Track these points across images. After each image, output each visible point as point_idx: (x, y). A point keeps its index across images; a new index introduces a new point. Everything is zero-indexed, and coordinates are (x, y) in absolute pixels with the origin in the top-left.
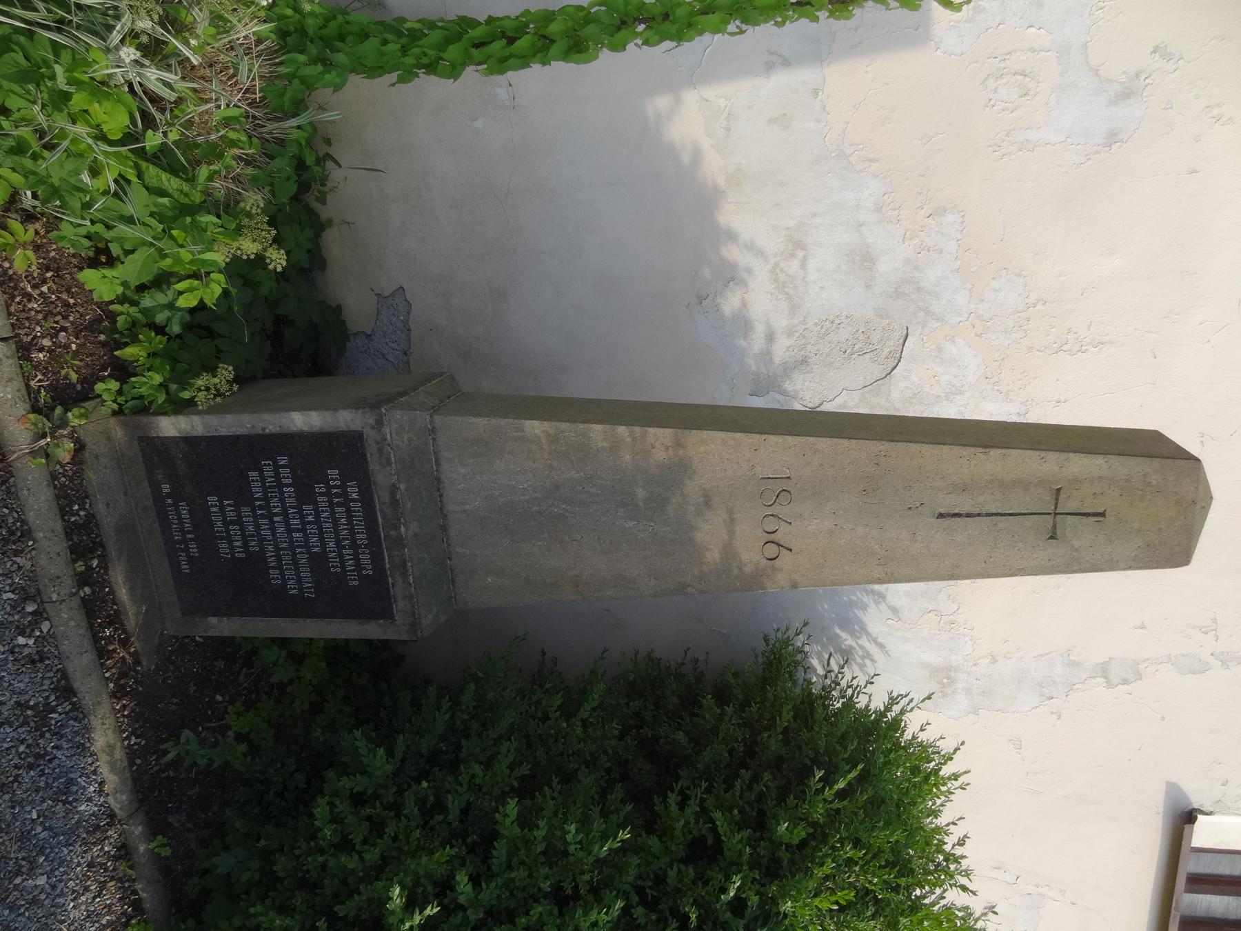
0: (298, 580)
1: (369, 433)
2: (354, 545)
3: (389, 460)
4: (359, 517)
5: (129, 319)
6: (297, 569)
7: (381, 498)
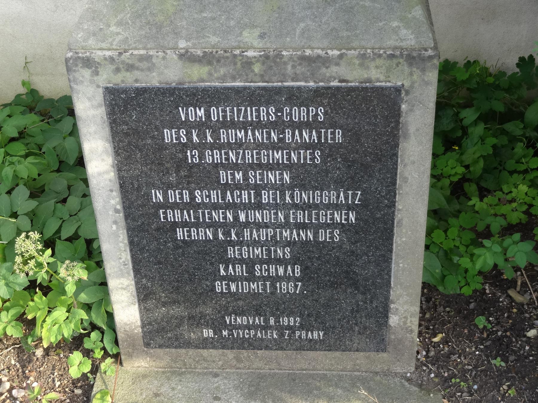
0: (335, 209)
1: (107, 77)
2: (278, 125)
3: (141, 58)
4: (232, 112)
5: (14, 323)
6: (316, 207)
7: (198, 76)
